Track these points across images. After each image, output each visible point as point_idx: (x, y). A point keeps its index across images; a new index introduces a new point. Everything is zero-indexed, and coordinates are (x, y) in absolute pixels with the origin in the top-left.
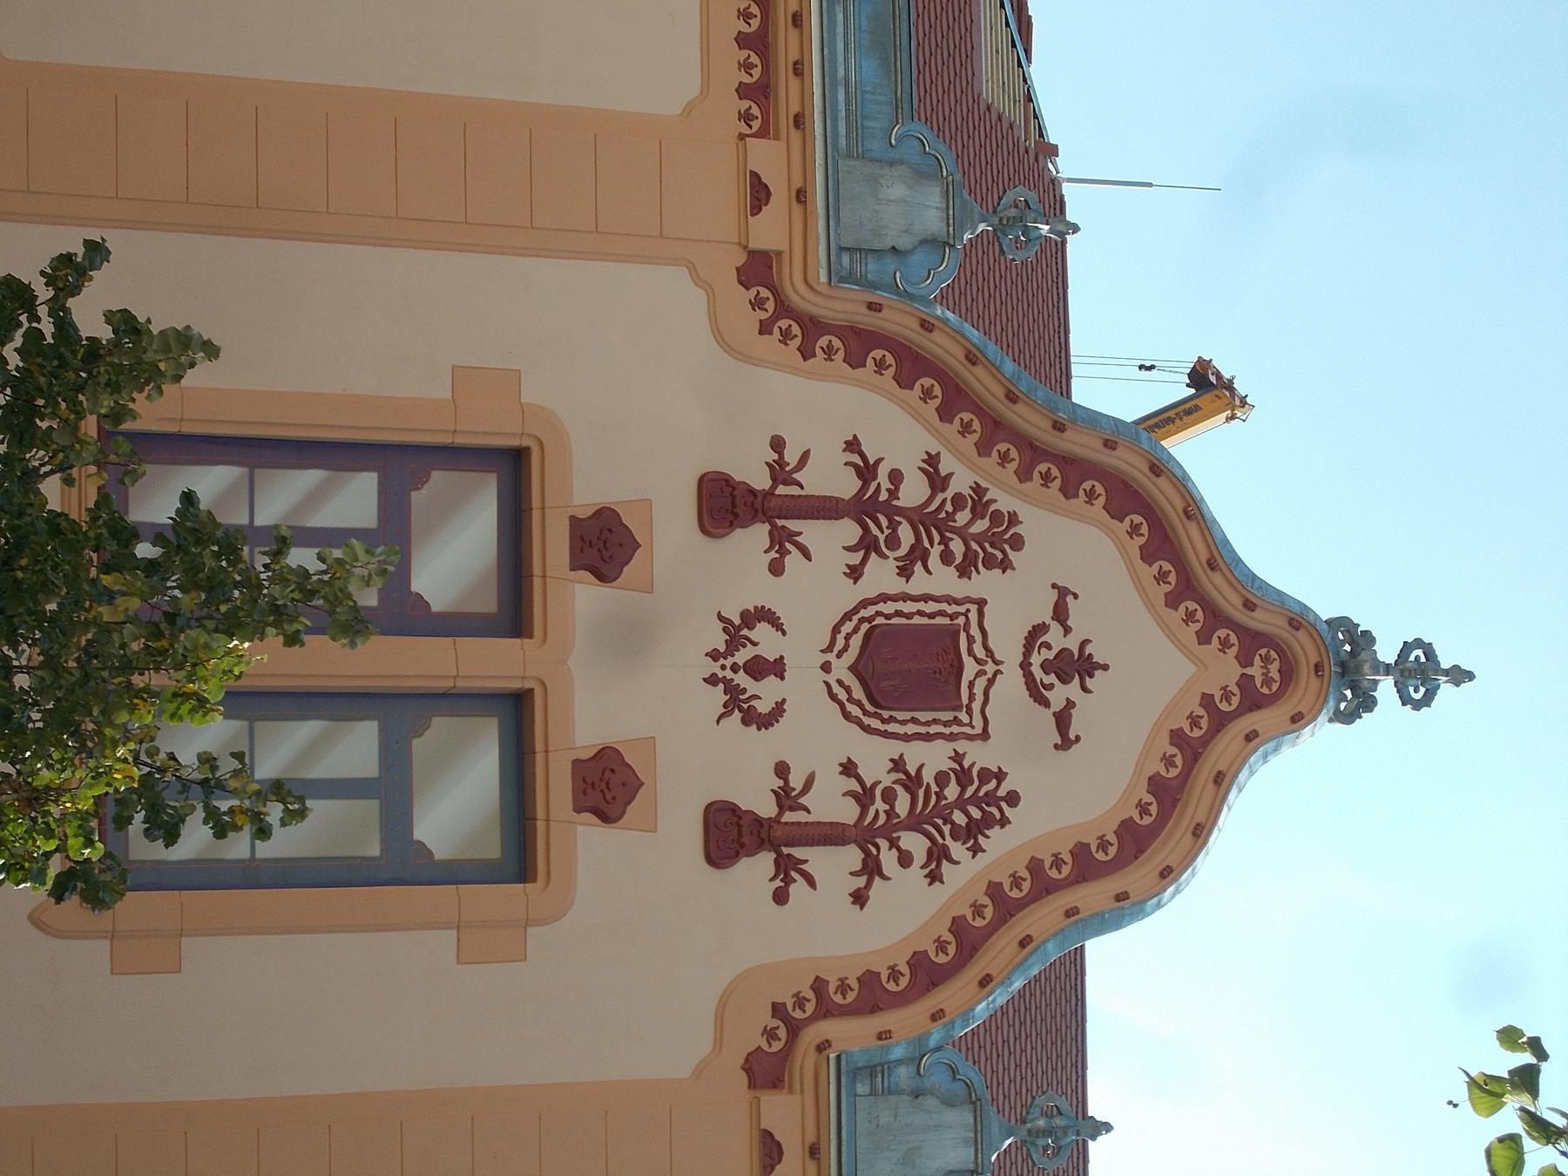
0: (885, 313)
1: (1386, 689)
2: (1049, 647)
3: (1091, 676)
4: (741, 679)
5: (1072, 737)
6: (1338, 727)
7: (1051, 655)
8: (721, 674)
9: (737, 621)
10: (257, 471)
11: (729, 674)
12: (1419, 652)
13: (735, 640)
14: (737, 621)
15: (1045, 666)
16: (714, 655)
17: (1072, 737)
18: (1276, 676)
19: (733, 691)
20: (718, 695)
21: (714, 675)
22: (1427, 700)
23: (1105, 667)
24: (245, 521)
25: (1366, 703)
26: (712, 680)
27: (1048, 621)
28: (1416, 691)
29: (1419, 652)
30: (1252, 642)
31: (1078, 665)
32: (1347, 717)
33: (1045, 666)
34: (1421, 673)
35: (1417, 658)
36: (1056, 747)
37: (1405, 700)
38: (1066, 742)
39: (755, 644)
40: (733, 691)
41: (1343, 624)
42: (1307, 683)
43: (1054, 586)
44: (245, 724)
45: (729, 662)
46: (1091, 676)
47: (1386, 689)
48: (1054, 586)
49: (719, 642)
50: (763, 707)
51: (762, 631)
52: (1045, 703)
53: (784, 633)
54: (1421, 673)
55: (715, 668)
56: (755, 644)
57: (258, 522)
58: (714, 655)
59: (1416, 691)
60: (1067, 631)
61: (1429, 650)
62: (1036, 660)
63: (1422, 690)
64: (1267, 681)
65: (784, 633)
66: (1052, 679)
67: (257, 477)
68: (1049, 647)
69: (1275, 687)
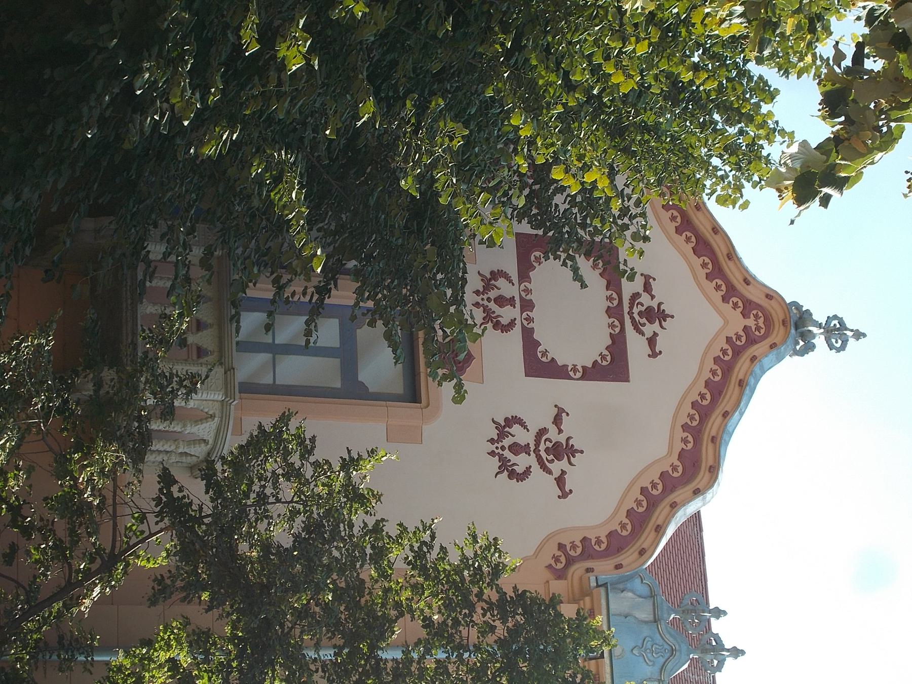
0: (612, 566)
1: (820, 341)
2: (642, 305)
3: (665, 321)
4: (492, 306)
5: (657, 351)
6: (796, 358)
7: (643, 309)
8: (481, 303)
9: (503, 424)
10: (277, 356)
11: (486, 303)
12: (836, 322)
13: (502, 434)
14: (503, 424)
15: (640, 314)
16: (492, 441)
17: (657, 351)
18: (762, 326)
19: (502, 459)
20: (495, 462)
21: (493, 451)
22: (843, 348)
23: (672, 317)
24: (271, 382)
25: (809, 348)
26: (492, 454)
27: (641, 291)
28: (837, 342)
29: (836, 322)
30: (748, 307)
31: (564, 451)
32: (811, 315)
33: (640, 314)
34: (838, 333)
35: (835, 325)
36: (559, 497)
37: (831, 347)
38: (564, 495)
39: (513, 436)
40: (502, 459)
41: (795, 304)
42: (778, 334)
43: (556, 406)
44: (270, 355)
45: (485, 297)
46: (665, 321)
47: (820, 341)
48: (556, 406)
49: (494, 434)
50: (520, 469)
51: (516, 429)
52: (550, 472)
53: (528, 430)
54: (838, 333)
55: (493, 447)
56: (513, 436)
57: (276, 342)
58: (492, 441)
59: (837, 342)
60: (653, 297)
61: (841, 322)
62: (542, 447)
63: (840, 342)
64: (758, 328)
65: (528, 430)
66: (644, 320)
67: (277, 361)
68: (642, 305)
69: (763, 331)
